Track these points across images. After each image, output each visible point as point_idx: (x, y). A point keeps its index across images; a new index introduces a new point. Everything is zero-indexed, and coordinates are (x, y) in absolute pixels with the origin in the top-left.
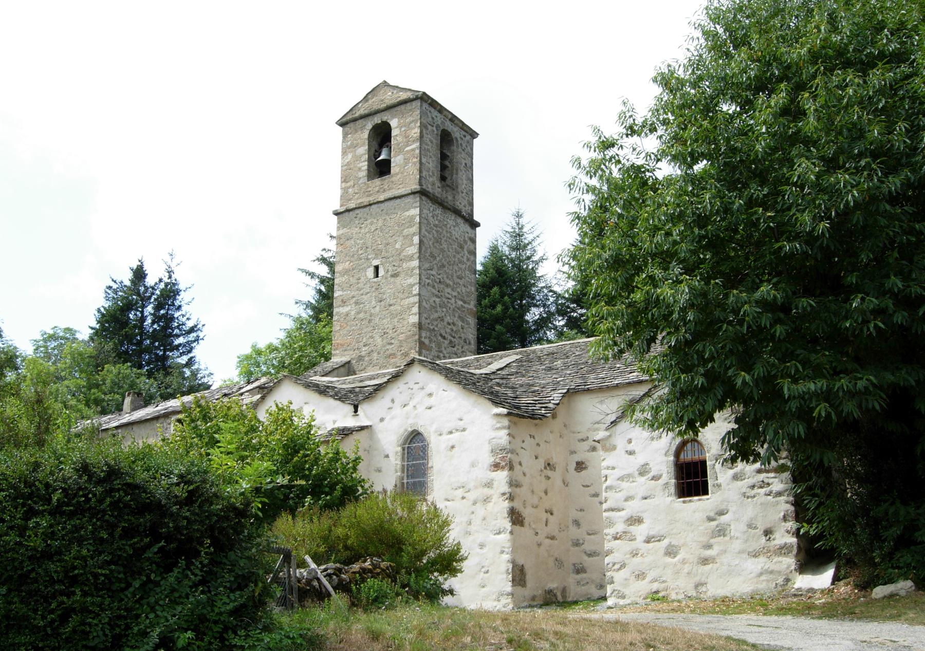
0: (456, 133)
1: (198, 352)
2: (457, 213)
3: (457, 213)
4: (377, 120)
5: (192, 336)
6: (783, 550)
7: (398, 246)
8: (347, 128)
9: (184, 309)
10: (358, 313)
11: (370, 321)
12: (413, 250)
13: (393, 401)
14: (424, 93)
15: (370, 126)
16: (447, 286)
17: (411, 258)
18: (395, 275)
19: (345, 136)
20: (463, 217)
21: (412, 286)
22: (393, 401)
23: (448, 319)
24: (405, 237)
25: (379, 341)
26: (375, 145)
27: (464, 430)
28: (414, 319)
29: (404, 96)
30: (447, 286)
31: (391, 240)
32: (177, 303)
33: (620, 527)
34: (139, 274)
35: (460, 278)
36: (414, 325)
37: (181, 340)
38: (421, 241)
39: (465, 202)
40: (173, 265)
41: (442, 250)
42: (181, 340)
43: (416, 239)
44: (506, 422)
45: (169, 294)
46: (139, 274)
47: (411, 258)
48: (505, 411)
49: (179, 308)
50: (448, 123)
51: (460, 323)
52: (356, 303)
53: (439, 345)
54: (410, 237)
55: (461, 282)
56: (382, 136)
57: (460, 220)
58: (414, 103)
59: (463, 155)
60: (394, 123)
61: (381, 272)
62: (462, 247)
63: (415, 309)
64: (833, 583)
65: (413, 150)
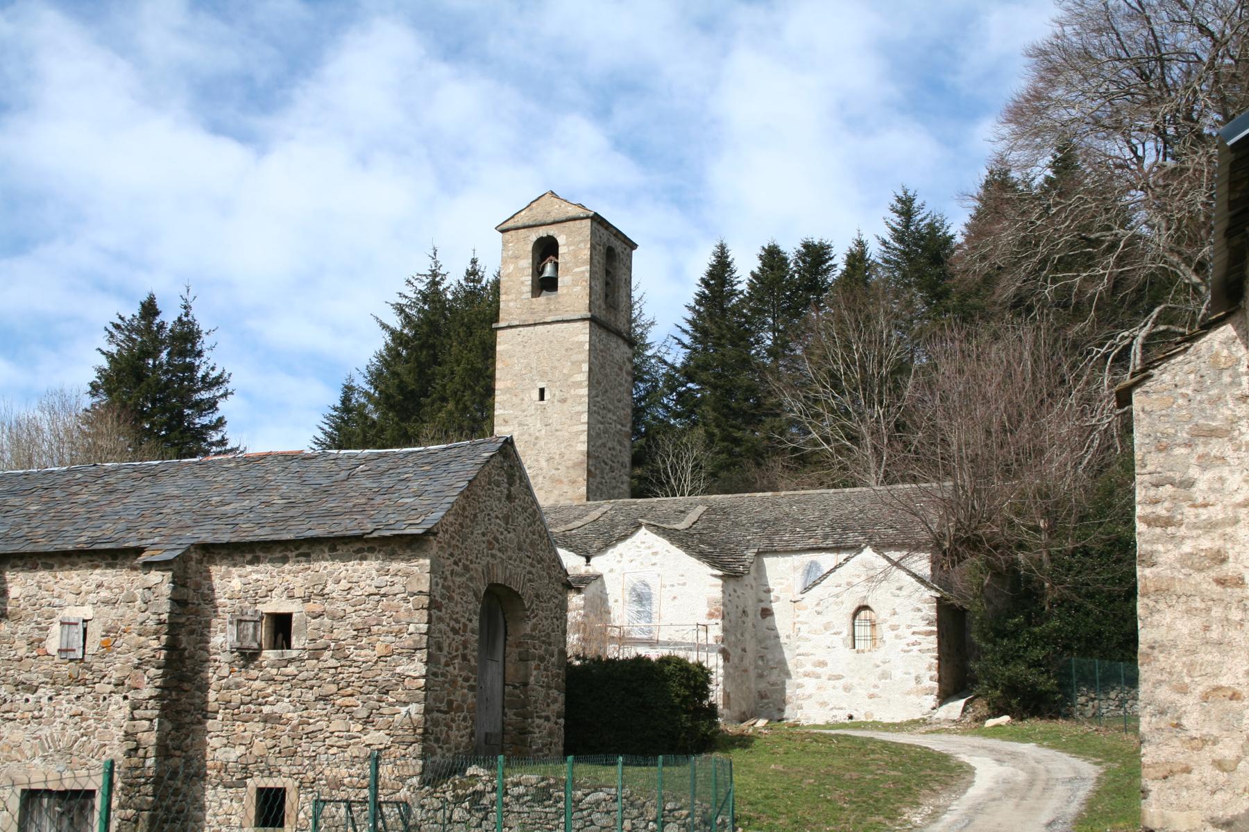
0: (618, 246)
1: (225, 408)
2: (619, 334)
3: (619, 334)
4: (542, 232)
5: (216, 392)
6: (928, 692)
7: (565, 371)
8: (508, 235)
9: (206, 354)
10: (522, 434)
11: (535, 444)
12: (583, 377)
13: (621, 555)
14: (596, 214)
15: (534, 238)
16: (609, 411)
17: (578, 385)
18: (564, 401)
19: (505, 244)
20: (623, 338)
21: (581, 413)
22: (621, 555)
23: (609, 445)
24: (573, 363)
25: (543, 464)
26: (538, 259)
27: (684, 584)
28: (584, 447)
29: (573, 211)
30: (609, 411)
31: (557, 364)
32: (198, 347)
33: (809, 668)
34: (149, 309)
35: (619, 401)
36: (582, 452)
37: (205, 395)
38: (590, 369)
39: (624, 321)
40: (190, 299)
41: (606, 375)
42: (205, 395)
43: (585, 367)
44: (720, 582)
45: (186, 338)
46: (149, 309)
47: (578, 385)
48: (720, 573)
49: (200, 354)
50: (612, 238)
51: (618, 447)
52: (520, 424)
53: (602, 472)
54: (577, 364)
55: (620, 405)
56: (546, 249)
57: (620, 342)
58: (584, 222)
59: (624, 270)
60: (561, 240)
61: (547, 396)
62: (621, 369)
63: (584, 437)
64: (350, 427)
65: (583, 272)
